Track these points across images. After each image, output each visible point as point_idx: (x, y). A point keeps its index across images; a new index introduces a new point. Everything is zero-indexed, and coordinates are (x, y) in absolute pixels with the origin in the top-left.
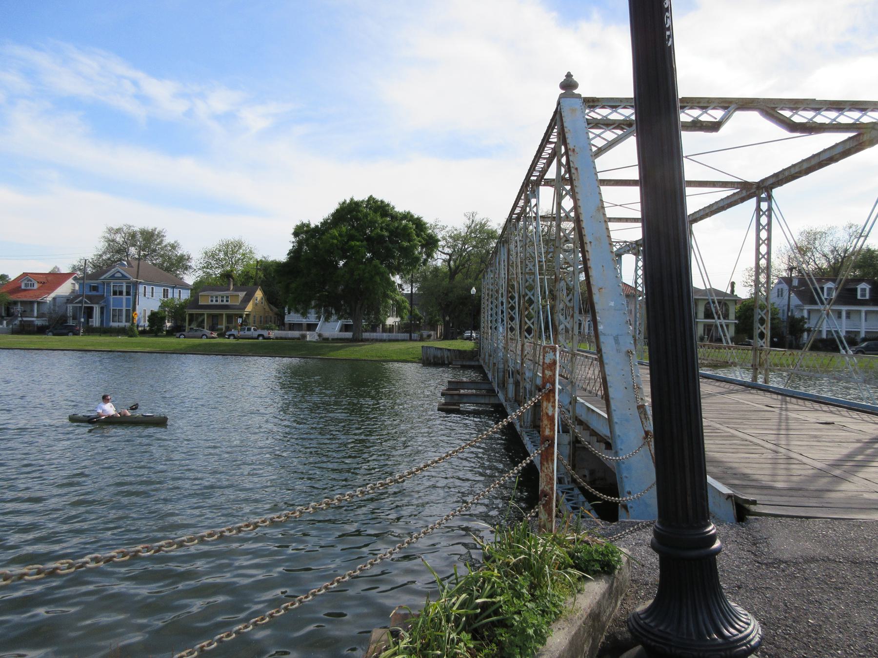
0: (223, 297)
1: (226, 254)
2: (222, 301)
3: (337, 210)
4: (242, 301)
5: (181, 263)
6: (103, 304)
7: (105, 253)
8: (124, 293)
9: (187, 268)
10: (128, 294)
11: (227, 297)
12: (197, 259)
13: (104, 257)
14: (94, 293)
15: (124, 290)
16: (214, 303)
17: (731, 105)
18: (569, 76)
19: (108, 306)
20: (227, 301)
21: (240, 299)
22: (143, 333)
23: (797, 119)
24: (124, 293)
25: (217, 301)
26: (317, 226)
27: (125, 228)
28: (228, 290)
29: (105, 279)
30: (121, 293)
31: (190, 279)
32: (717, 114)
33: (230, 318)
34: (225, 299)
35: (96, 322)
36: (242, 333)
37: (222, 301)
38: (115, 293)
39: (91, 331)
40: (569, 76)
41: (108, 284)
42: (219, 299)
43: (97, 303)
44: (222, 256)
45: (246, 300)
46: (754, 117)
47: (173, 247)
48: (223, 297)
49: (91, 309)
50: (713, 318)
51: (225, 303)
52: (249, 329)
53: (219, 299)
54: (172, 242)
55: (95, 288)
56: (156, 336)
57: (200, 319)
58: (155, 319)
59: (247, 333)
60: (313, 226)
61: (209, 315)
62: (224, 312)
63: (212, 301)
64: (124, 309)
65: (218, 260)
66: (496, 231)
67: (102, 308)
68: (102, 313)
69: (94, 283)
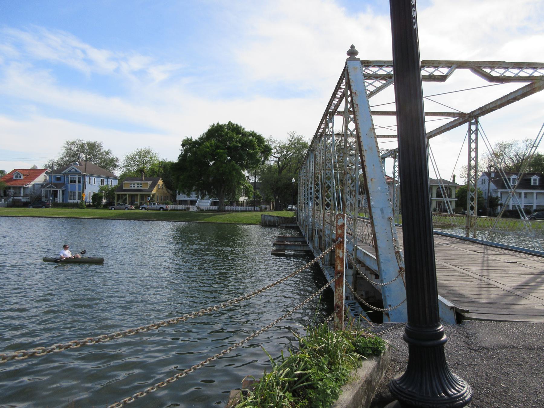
0: (138, 184)
1: (140, 157)
2: (138, 187)
3: (209, 130)
4: (150, 187)
5: (112, 163)
6: (64, 189)
7: (65, 157)
8: (77, 182)
9: (116, 166)
10: (79, 182)
11: (141, 184)
12: (122, 160)
13: (65, 160)
14: (58, 182)
15: (77, 180)
16: (133, 188)
17: (453, 65)
18: (352, 47)
19: (67, 190)
20: (141, 187)
21: (149, 186)
22: (89, 206)
23: (494, 74)
24: (77, 182)
25: (134, 187)
26: (196, 140)
27: (77, 141)
28: (141, 180)
29: (65, 173)
30: (75, 182)
31: (118, 173)
32: (444, 71)
33: (142, 197)
34: (139, 186)
35: (59, 199)
36: (150, 206)
37: (138, 187)
38: (71, 182)
39: (56, 205)
40: (352, 47)
41: (67, 176)
42: (136, 186)
43: (60, 188)
44: (137, 158)
45: (153, 186)
46: (467, 73)
47: (107, 153)
48: (138, 184)
49: (57, 191)
50: (442, 197)
51: (139, 188)
52: (154, 204)
53: (136, 186)
54: (107, 150)
55: (59, 179)
56: (97, 208)
57: (124, 198)
58: (96, 198)
59: (153, 206)
60: (194, 140)
61: (129, 195)
62: (139, 193)
63: (131, 187)
64: (77, 191)
65: (135, 161)
66: (307, 143)
67: (63, 191)
68: (63, 194)
69: (58, 175)
